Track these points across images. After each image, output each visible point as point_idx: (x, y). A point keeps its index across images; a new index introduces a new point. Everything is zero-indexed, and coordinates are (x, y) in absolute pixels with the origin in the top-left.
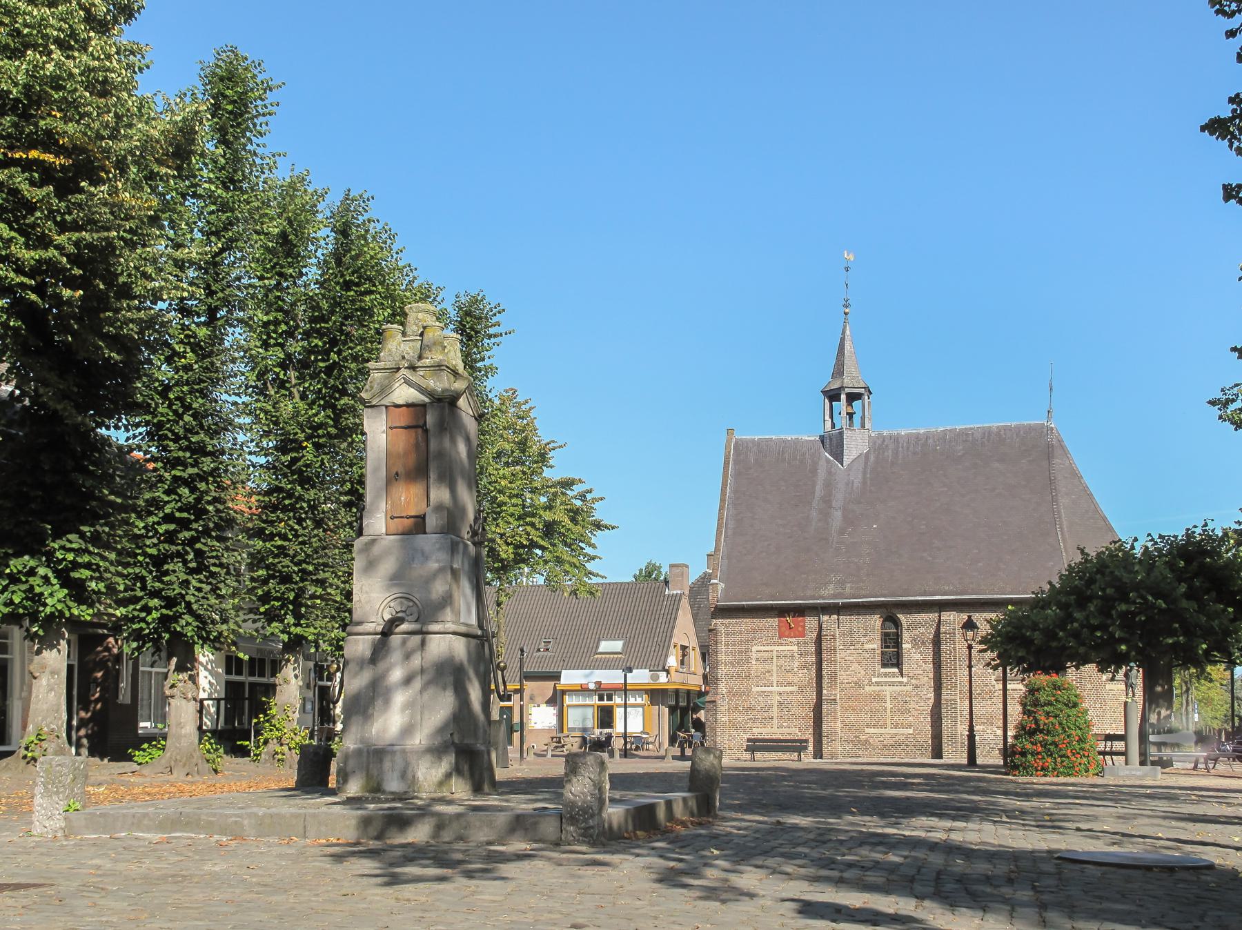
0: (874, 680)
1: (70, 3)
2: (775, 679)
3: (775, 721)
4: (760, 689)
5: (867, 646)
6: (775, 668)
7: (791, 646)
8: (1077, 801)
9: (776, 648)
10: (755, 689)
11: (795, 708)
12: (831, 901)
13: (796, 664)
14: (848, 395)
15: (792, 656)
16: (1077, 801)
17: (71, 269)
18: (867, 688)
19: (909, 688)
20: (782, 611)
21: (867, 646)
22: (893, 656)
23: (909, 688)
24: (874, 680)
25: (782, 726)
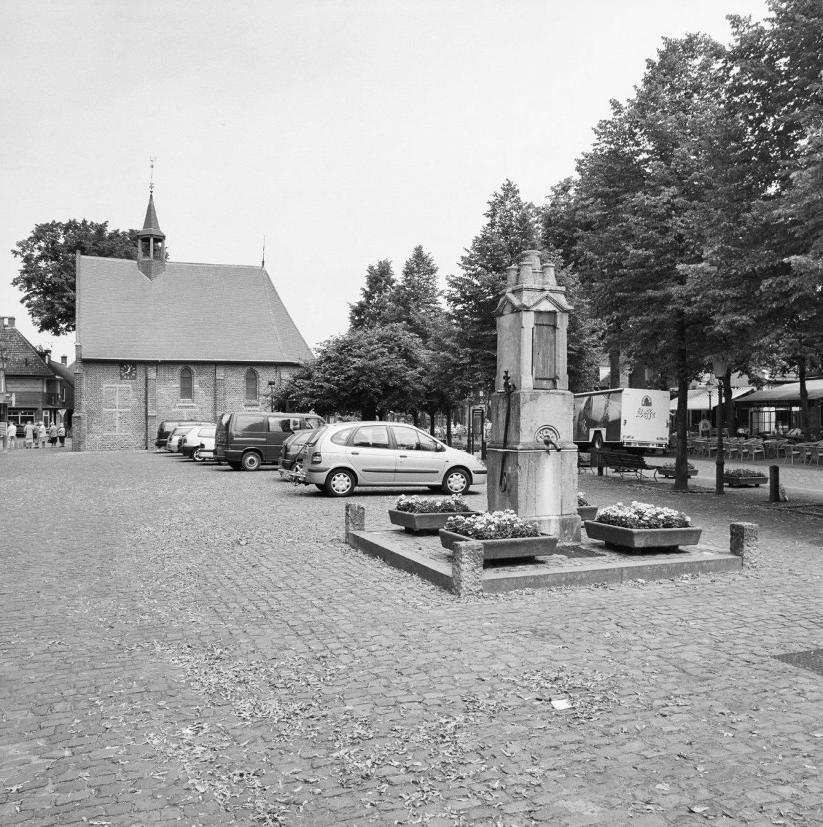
0: (178, 405)
1: (820, 341)
2: (117, 404)
3: (117, 429)
4: (107, 410)
5: (174, 386)
6: (117, 397)
7: (127, 385)
8: (386, 488)
9: (117, 386)
10: (104, 410)
11: (129, 421)
12: (517, 556)
13: (131, 395)
14: (154, 239)
15: (128, 391)
16: (386, 488)
17: (726, 389)
18: (174, 410)
19: (197, 410)
20: (122, 363)
21: (174, 386)
22: (187, 391)
23: (197, 410)
24: (178, 405)
25: (121, 431)
